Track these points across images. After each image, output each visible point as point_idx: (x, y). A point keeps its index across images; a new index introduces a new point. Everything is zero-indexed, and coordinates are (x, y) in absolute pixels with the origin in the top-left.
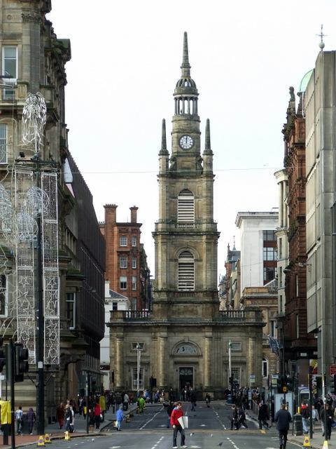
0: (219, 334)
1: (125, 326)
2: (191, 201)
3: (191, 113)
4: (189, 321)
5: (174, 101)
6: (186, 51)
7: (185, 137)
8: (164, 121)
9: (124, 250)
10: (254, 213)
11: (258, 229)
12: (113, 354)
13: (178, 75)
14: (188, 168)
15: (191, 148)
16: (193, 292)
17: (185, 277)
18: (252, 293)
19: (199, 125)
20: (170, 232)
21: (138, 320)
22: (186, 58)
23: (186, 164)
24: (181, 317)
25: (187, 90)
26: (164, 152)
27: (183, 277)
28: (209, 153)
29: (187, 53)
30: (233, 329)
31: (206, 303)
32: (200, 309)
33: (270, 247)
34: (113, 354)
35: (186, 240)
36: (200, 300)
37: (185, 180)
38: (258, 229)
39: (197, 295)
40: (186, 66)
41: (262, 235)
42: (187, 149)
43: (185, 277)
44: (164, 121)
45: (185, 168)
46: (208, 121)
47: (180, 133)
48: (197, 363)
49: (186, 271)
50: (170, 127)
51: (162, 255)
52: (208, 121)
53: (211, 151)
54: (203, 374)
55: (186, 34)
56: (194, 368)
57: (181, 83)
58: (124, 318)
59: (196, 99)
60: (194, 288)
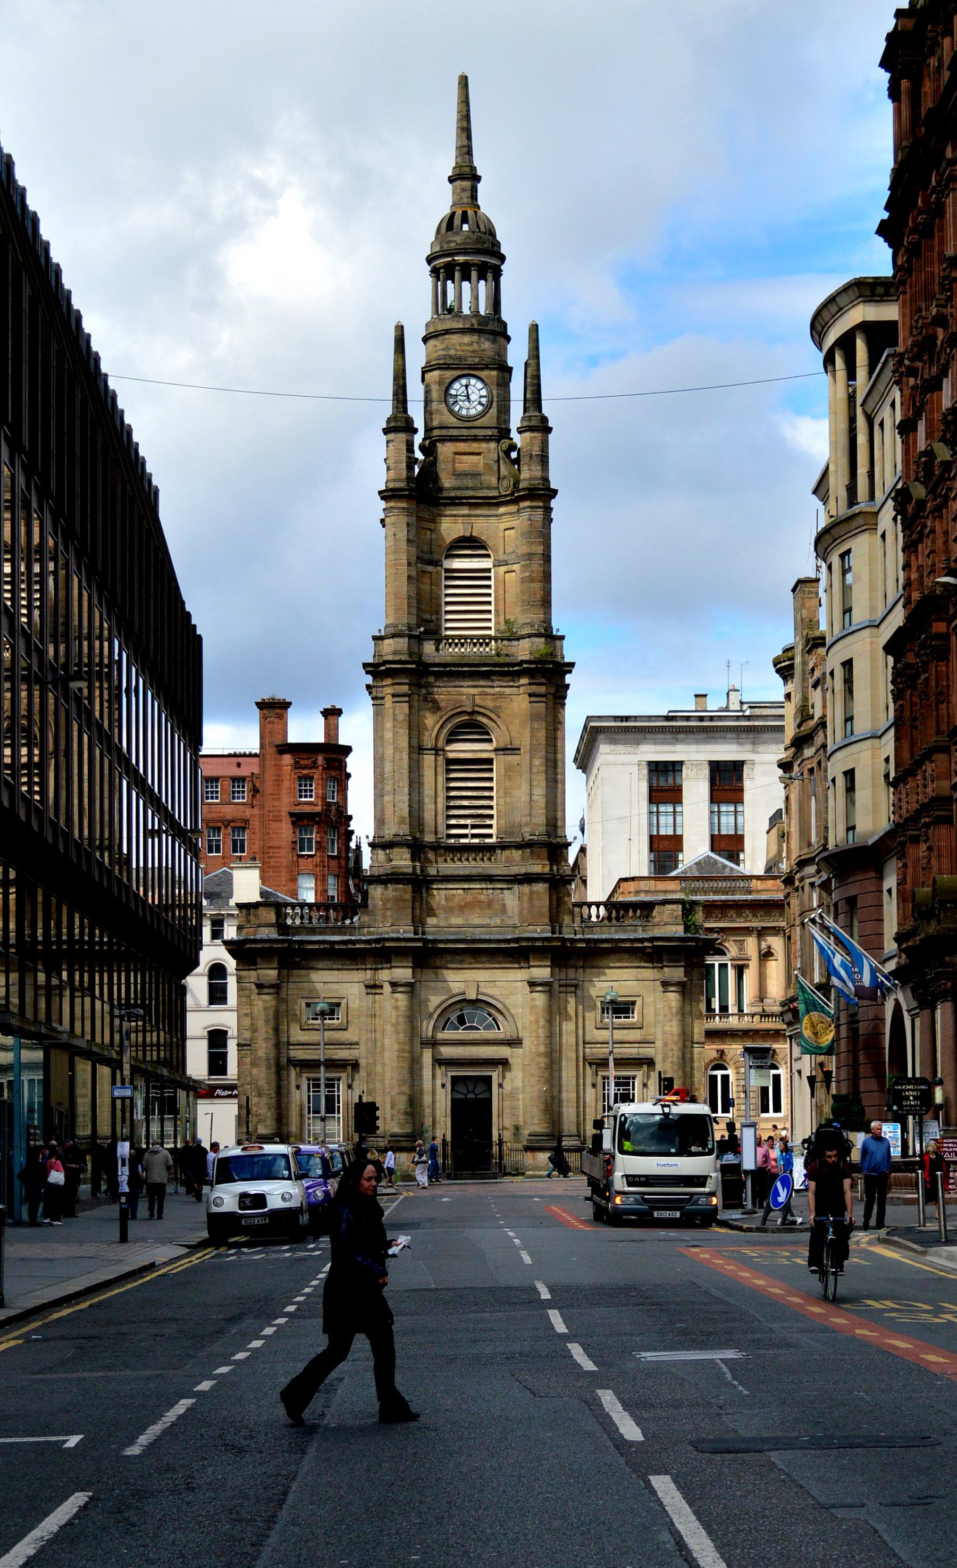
0: (571, 973)
1: (279, 953)
2: (483, 574)
3: (482, 312)
4: (480, 934)
5: (429, 281)
6: (465, 130)
7: (464, 381)
8: (400, 330)
9: (308, 809)
10: (627, 718)
11: (635, 759)
12: (247, 1035)
13: (442, 201)
14: (475, 475)
15: (482, 415)
16: (491, 849)
17: (465, 803)
18: (637, 892)
19: (505, 349)
20: (411, 671)
21: (322, 932)
22: (466, 150)
23: (466, 463)
24: (455, 921)
25: (468, 252)
26: (399, 425)
27: (458, 803)
28: (540, 426)
29: (469, 138)
30: (766, 736)
31: (529, 879)
32: (511, 898)
33: (665, 802)
34: (247, 1035)
35: (467, 693)
36: (515, 870)
37: (465, 511)
38: (635, 759)
39: (502, 855)
40: (466, 176)
41: (645, 771)
42: (469, 419)
43: (465, 803)
44: (400, 330)
45: (465, 474)
46: (534, 330)
47: (448, 368)
48: (504, 1063)
49: (465, 781)
50: (416, 356)
51: (395, 734)
52: (534, 330)
53: (544, 419)
54: (516, 1102)
55: (464, 82)
56: (495, 1075)
57: (449, 224)
58: (282, 927)
59: (497, 274)
60: (494, 834)
